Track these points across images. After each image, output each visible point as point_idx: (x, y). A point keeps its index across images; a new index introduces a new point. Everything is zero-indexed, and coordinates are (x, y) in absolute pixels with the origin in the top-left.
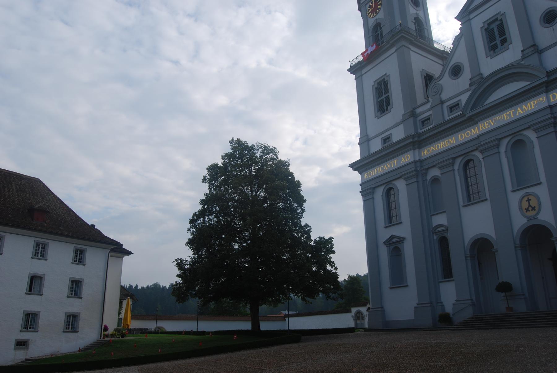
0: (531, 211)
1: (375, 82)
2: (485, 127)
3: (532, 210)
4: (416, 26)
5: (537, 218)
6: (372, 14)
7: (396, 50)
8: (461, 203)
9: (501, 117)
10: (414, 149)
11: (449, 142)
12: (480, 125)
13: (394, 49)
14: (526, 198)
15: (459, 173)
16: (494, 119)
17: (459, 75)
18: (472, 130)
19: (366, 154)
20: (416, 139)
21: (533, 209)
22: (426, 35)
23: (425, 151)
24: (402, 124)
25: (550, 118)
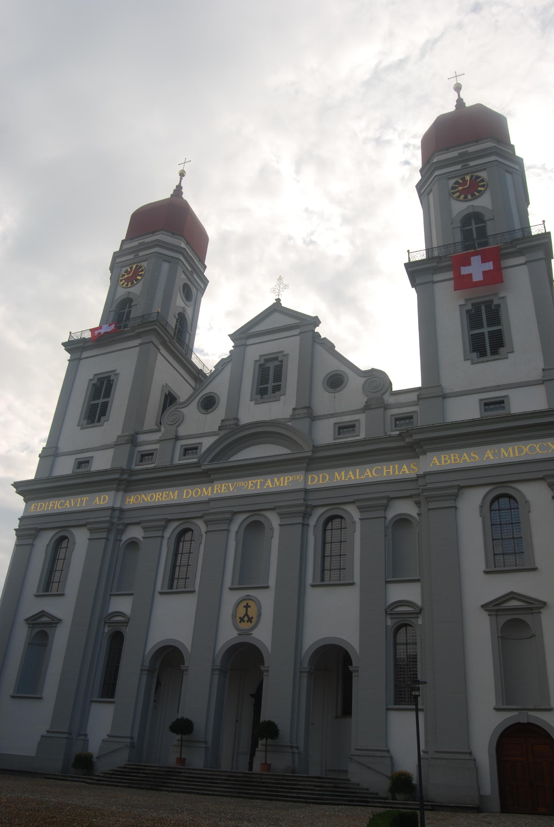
0: (246, 622)
1: (95, 375)
2: (162, 499)
3: (247, 621)
4: (178, 324)
5: (251, 634)
6: (126, 283)
7: (140, 345)
8: (159, 588)
9: (245, 484)
10: (118, 490)
11: (168, 495)
12: (216, 486)
13: (137, 342)
14: (244, 603)
15: (236, 536)
16: (235, 483)
17: (210, 410)
18: (142, 496)
20: (125, 477)
21: (250, 620)
22: (187, 341)
23: (132, 498)
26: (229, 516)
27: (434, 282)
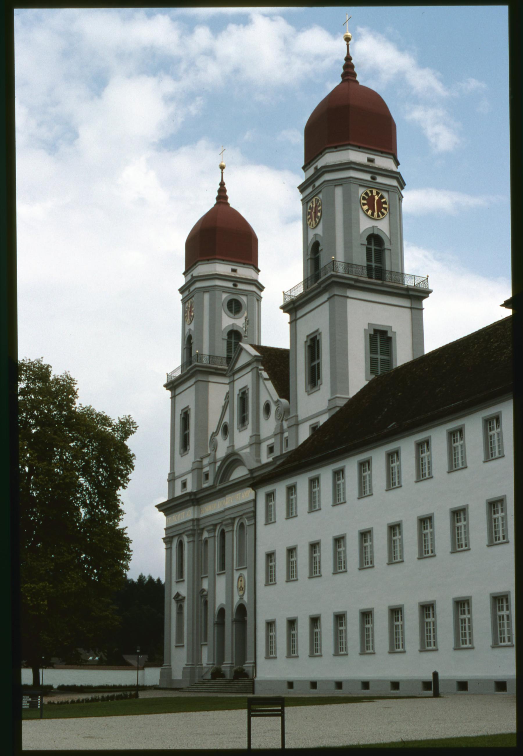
1: (308, 336)
8: (217, 572)
19: (171, 498)
20: (193, 497)
26: (230, 521)
27: (348, 297)
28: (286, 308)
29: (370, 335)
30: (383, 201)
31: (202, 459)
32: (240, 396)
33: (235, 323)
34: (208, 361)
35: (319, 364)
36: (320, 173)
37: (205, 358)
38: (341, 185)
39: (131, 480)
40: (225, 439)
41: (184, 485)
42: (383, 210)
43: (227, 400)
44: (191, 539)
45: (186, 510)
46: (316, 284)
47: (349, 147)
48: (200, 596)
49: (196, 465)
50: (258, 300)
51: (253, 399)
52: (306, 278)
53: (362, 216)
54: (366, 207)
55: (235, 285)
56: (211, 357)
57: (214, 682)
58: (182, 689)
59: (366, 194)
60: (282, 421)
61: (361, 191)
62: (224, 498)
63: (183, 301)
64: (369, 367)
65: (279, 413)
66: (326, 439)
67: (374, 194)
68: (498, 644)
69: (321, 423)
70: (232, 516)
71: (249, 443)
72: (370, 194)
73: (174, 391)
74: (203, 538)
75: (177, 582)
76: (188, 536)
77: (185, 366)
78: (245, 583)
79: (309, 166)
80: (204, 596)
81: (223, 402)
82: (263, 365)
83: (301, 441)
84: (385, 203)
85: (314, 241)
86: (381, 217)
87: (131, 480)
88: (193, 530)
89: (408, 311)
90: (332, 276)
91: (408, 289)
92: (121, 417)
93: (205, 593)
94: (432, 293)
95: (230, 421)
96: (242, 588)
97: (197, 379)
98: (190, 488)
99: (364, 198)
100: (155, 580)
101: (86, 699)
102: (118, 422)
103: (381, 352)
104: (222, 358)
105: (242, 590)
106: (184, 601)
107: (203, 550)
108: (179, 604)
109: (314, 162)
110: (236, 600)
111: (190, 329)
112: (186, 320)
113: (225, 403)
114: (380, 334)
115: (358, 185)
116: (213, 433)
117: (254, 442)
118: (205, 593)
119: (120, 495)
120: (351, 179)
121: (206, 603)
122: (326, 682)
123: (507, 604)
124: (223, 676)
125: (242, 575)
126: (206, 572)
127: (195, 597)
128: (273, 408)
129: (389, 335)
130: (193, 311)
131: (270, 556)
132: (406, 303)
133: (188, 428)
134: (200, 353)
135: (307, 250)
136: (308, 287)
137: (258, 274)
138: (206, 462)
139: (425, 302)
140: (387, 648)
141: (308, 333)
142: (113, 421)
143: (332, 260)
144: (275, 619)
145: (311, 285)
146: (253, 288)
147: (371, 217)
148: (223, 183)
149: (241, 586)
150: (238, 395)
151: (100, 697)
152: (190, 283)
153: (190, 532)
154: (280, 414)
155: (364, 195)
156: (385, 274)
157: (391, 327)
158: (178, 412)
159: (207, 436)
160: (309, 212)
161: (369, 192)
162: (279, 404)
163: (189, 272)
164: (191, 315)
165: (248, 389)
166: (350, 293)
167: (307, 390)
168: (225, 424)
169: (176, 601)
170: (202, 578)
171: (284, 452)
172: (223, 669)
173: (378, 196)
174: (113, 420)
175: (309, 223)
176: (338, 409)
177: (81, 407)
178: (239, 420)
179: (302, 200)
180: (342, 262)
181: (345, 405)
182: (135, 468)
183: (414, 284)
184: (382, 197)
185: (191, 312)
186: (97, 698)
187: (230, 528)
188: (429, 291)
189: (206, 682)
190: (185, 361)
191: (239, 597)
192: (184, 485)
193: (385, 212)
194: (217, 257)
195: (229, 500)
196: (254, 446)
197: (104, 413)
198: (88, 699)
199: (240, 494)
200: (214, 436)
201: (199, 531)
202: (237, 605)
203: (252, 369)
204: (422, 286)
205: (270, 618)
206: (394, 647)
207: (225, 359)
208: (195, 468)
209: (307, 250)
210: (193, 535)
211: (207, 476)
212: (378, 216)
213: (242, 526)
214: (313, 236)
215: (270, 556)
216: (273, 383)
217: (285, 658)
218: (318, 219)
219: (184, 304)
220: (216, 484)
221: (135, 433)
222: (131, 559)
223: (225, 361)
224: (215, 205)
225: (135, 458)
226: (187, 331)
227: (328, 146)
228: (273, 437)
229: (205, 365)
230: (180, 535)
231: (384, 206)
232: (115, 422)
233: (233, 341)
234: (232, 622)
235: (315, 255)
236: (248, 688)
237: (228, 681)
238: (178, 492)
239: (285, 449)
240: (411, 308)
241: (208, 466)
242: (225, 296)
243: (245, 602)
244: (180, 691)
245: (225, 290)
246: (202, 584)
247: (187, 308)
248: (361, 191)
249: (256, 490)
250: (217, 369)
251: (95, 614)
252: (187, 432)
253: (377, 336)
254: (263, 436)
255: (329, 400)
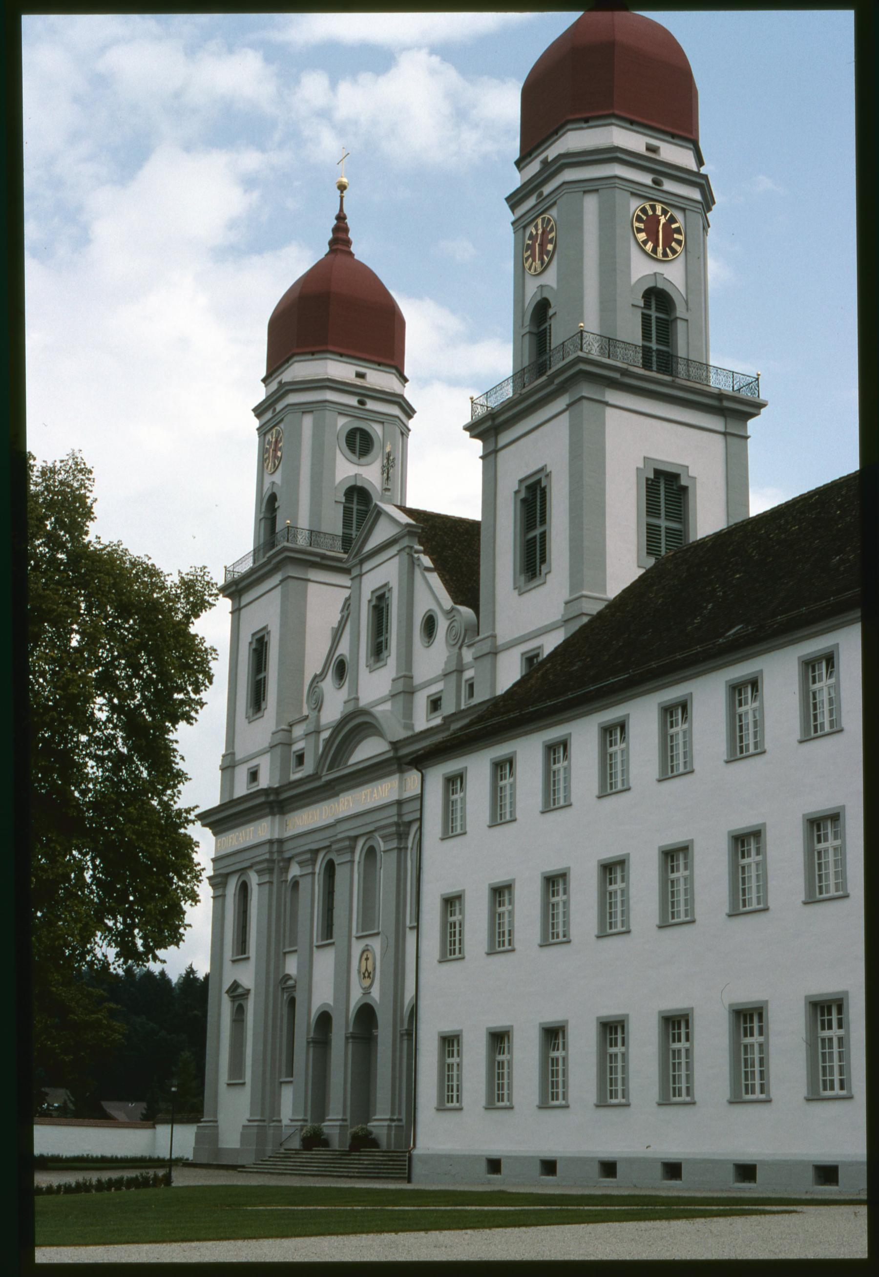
7: (569, 406)
8: (315, 943)
13: (561, 403)
19: (227, 800)
20: (272, 798)
24: (269, 754)
25: (267, 860)
27: (607, 404)
28: (479, 429)
29: (647, 479)
30: (673, 226)
31: (291, 726)
32: (374, 603)
33: (360, 473)
34: (309, 542)
35: (543, 535)
36: (553, 168)
37: (303, 534)
38: (597, 190)
39: (206, 703)
40: (340, 687)
41: (254, 776)
42: (674, 244)
43: (346, 613)
44: (266, 878)
45: (257, 823)
46: (544, 378)
47: (614, 121)
48: (280, 988)
49: (280, 737)
50: (402, 434)
51: (399, 608)
52: (520, 368)
53: (635, 251)
54: (642, 236)
55: (361, 403)
56: (314, 534)
57: (308, 1156)
58: (243, 1167)
59: (644, 210)
60: (460, 648)
61: (635, 205)
62: (335, 799)
63: (261, 430)
64: (645, 543)
65: (454, 632)
66: (575, 668)
67: (659, 212)
68: (819, 1094)
69: (548, 650)
70: (353, 833)
71: (390, 691)
72: (650, 213)
73: (237, 599)
74: (290, 877)
75: (234, 961)
76: (260, 872)
77: (262, 551)
78: (374, 964)
79: (529, 159)
80: (288, 988)
81: (338, 617)
82: (421, 544)
83: (613, 590)
84: (678, 231)
85: (539, 298)
86: (671, 257)
87: (206, 703)
88: (271, 861)
89: (719, 440)
90: (579, 360)
91: (720, 396)
92: (185, 571)
93: (291, 982)
94: (767, 407)
95: (351, 651)
96: (369, 974)
97: (286, 575)
98: (264, 782)
99: (639, 219)
100: (157, 973)
101: (65, 1185)
102: (177, 580)
103: (666, 515)
104: (333, 536)
105: (369, 977)
106: (247, 998)
107: (288, 900)
108: (236, 1004)
109: (541, 149)
110: (356, 997)
111: (273, 483)
112: (266, 465)
113: (342, 617)
114: (666, 480)
115: (629, 193)
116: (316, 676)
117: (401, 689)
118: (291, 982)
119: (177, 742)
120: (617, 181)
121: (292, 1002)
122: (710, 1164)
123: (840, 1016)
124: (325, 1143)
125: (369, 948)
126: (293, 942)
127: (271, 989)
128: (442, 625)
129: (684, 482)
130: (280, 449)
131: (451, 902)
132: (716, 423)
133: (265, 668)
134: (291, 525)
135: (523, 317)
136: (524, 384)
137: (404, 386)
138: (299, 731)
139: (752, 425)
140: (535, 1099)
141: (522, 475)
142: (167, 578)
143: (578, 331)
144: (461, 1031)
145: (530, 383)
146: (395, 411)
147: (652, 256)
148: (342, 215)
149: (366, 970)
150: (370, 601)
151: (94, 1182)
152: (275, 397)
153: (265, 865)
154: (456, 635)
155: (640, 214)
156: (677, 363)
157: (687, 467)
158: (246, 639)
159: (302, 684)
160: (528, 245)
161: (648, 207)
162: (454, 616)
163: (274, 376)
164: (275, 457)
165: (390, 590)
166: (613, 396)
167: (517, 585)
168: (340, 658)
169: (231, 997)
170: (285, 953)
171: (463, 707)
172: (325, 1130)
173: (665, 217)
174: (168, 575)
175: (527, 265)
176: (585, 620)
177: (99, 543)
178: (518, 523)
179: (513, 223)
180: (598, 335)
181: (600, 614)
182: (214, 679)
183: (733, 387)
184: (672, 220)
185: (275, 451)
186: (88, 1184)
187: (347, 858)
188: (762, 402)
189: (292, 1156)
190: (262, 541)
191: (361, 991)
192: (254, 776)
193: (678, 249)
194: (331, 348)
195: (346, 803)
196: (401, 698)
197: (150, 558)
198: (70, 1186)
199: (369, 790)
200: (318, 683)
201: (281, 864)
202: (317, 1015)
203: (399, 551)
204: (745, 394)
205: (448, 1028)
206: (741, 1092)
207: (340, 538)
208: (276, 743)
209: (523, 317)
210: (271, 871)
211: (300, 759)
212: (665, 254)
213: (371, 853)
214: (535, 290)
215: (451, 902)
216: (442, 577)
217: (434, 1111)
218: (547, 257)
219: (262, 437)
220: (322, 772)
221: (213, 608)
222: (200, 878)
223: (339, 543)
224: (326, 255)
225: (216, 657)
226: (267, 485)
227: (572, 117)
228: (441, 680)
229: (301, 547)
230: (243, 871)
231: (676, 236)
232: (172, 580)
233: (355, 507)
234: (347, 1038)
235: (539, 327)
236: (381, 1169)
237: (338, 1155)
238: (241, 789)
239: (465, 702)
240: (725, 434)
241: (303, 739)
242: (343, 423)
243: (376, 1001)
244: (240, 1172)
245: (343, 410)
246: (284, 967)
247: (268, 444)
248: (635, 205)
249: (423, 771)
250: (324, 557)
251: (76, 1018)
252: (262, 676)
253: (659, 482)
254: (418, 680)
255: (566, 603)
